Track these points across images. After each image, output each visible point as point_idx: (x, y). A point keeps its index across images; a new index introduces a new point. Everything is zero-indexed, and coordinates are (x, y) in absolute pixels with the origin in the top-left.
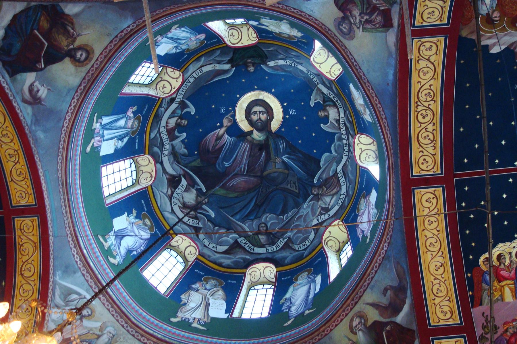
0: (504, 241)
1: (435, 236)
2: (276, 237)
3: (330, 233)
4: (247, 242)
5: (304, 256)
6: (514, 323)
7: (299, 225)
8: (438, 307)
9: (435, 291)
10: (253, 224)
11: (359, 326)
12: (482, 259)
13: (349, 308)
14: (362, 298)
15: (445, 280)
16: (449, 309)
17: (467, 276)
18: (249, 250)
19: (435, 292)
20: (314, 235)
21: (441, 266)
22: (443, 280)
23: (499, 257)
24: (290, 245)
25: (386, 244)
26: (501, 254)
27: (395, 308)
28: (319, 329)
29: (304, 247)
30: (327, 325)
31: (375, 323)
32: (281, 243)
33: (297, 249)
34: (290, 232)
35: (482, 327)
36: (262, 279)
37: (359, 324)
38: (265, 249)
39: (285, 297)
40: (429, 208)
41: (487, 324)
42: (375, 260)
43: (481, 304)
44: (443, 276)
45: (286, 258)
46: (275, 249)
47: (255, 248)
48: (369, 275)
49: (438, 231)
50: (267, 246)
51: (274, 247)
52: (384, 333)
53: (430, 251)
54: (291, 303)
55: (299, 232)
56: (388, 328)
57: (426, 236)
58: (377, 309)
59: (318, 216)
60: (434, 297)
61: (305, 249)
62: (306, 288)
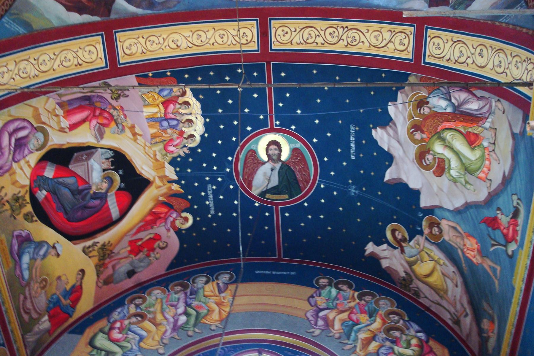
0: (203, 108)
1: (208, 40)
6: (122, 116)
8: (136, 41)
9: (152, 38)
15: (163, 49)
16: (134, 52)
19: (150, 39)
21: (177, 46)
22: (163, 47)
23: (187, 103)
26: (190, 104)
49: (213, 44)
53: (193, 34)
57: (208, 31)
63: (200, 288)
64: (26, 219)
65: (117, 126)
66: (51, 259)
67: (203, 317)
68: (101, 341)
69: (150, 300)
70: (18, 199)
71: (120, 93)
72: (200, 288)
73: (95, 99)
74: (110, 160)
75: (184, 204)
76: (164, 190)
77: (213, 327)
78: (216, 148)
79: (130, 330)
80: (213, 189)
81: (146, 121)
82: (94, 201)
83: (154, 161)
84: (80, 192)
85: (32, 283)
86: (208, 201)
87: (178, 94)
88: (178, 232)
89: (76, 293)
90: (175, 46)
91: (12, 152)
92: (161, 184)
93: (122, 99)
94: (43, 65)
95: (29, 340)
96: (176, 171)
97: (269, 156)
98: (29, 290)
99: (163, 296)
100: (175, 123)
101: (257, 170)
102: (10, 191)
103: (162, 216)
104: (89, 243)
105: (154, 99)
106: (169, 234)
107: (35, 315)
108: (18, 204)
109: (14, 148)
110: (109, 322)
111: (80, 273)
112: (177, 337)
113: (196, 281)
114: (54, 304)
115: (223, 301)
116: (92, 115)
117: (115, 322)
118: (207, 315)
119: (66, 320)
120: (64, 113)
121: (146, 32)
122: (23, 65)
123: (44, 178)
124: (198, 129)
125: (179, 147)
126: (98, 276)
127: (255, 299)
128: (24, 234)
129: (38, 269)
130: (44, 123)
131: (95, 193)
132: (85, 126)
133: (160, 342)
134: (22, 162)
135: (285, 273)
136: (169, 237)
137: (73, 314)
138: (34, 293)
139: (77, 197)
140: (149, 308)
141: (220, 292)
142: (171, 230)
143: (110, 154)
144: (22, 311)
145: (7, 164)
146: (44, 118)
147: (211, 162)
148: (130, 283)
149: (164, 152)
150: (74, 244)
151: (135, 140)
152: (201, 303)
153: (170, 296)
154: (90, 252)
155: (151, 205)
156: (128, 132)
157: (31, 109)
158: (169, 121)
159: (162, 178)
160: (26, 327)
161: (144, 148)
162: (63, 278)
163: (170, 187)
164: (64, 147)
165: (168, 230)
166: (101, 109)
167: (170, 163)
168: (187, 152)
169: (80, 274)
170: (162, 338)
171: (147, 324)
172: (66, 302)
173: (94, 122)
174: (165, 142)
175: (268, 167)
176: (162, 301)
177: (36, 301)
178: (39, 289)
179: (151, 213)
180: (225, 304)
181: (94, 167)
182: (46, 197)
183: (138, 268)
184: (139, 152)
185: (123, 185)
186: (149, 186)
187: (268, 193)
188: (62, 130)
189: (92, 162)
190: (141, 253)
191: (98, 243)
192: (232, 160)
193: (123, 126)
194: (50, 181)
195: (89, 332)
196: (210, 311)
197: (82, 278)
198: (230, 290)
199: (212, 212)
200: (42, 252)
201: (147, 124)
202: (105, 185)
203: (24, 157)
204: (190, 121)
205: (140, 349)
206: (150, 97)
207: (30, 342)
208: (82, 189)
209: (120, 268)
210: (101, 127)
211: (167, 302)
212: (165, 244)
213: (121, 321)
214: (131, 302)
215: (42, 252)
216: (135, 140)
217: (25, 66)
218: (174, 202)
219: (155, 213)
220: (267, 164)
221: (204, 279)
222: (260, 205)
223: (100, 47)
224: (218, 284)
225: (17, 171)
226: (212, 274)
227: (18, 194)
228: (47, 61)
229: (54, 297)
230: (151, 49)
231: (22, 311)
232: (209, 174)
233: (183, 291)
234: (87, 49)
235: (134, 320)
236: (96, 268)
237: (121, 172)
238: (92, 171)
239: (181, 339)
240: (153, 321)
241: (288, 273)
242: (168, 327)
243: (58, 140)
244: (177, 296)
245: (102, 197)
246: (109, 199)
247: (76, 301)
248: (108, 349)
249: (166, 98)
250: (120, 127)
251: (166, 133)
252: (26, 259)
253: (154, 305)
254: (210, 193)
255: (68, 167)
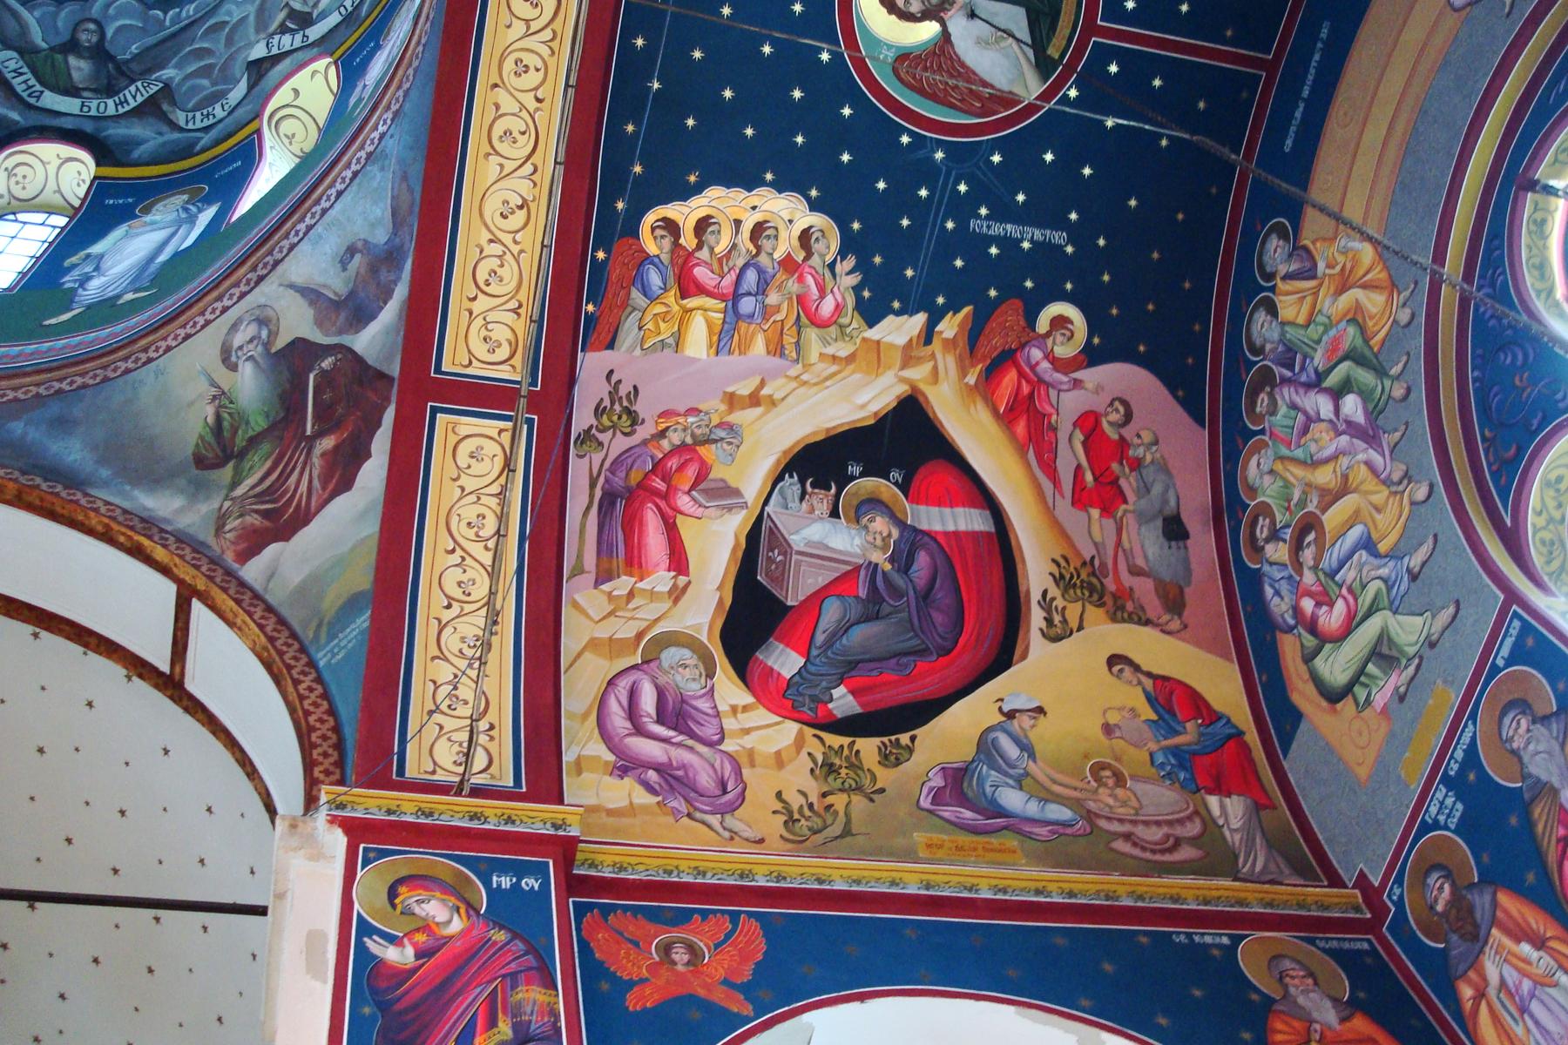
0: (728, 183)
1: (524, 114)
2: (123, 74)
3: (296, 92)
4: (25, 70)
5: (198, 148)
6: (691, 419)
7: (208, 52)
8: (479, 322)
9: (482, 276)
10: (56, 14)
11: (251, 347)
12: (650, 218)
13: (236, 291)
14: (280, 268)
15: (522, 251)
16: (509, 335)
17: (593, 257)
18: (24, 95)
19: (481, 279)
20: (244, 91)
21: (521, 207)
23: (703, 225)
24: (165, 107)
25: (389, 115)
26: (710, 217)
27: (358, 312)
28: (133, 342)
29: (206, 123)
30: (162, 332)
31: (299, 344)
32: (135, 95)
33: (182, 123)
34: (175, 67)
35: (596, 409)
36: (49, 196)
37: (251, 341)
38: (78, 102)
39: (89, 251)
40: (527, 21)
41: (612, 403)
42: (345, 159)
43: (611, 345)
44: (518, 237)
45: (139, 143)
46: (111, 111)
47: (47, 93)
48: (318, 202)
49: (539, 100)
50: (85, 94)
51: (110, 102)
52: (312, 377)
53: (498, 154)
54: (97, 269)
55: (205, 71)
56: (327, 364)
57: (497, 107)
58: (312, 303)
59: (271, 35)
60: (473, 292)
61: (206, 129)
62: (159, 236)
63: (1283, 333)
64: (898, 762)
65: (715, 441)
66: (1042, 733)
67: (1366, 341)
68: (1336, 666)
69: (1269, 492)
70: (832, 765)
71: (621, 408)
72: (1283, 333)
73: (618, 481)
74: (809, 489)
75: (1010, 315)
76: (948, 363)
77: (1404, 317)
78: (861, 175)
79: (1332, 575)
80: (987, 217)
81: (724, 358)
82: (915, 567)
83: (852, 367)
84: (874, 595)
85: (1092, 805)
86: (1022, 240)
87: (667, 243)
88: (1092, 356)
89: (1173, 700)
90: (522, 214)
91: (690, 742)
92: (928, 366)
93: (639, 407)
94: (470, 589)
95: (1258, 868)
96: (898, 313)
97: (926, 15)
98: (1109, 819)
99: (1270, 452)
100: (751, 276)
101: (963, 65)
102: (799, 781)
103: (1026, 389)
104: (1037, 617)
105: (664, 317)
106: (1089, 385)
107: (1193, 829)
108: (843, 771)
109: (681, 733)
110: (1290, 629)
111: (1116, 669)
112: (1397, 435)
113: (1258, 342)
114: (1182, 766)
115: (1338, 268)
116: (662, 504)
117: (1297, 610)
118: (1362, 330)
119: (1246, 748)
120: (631, 575)
121: (460, 287)
122: (451, 641)
123: (797, 678)
124: (788, 212)
125: (829, 283)
126: (1147, 623)
127: (1365, 165)
128: (938, 782)
129: (1058, 777)
130: (640, 636)
131: (892, 560)
132: (686, 527)
133: (1394, 489)
134: (729, 724)
135: (1317, 57)
136: (1099, 389)
137: (1235, 727)
138: (1121, 810)
139: (886, 609)
140: (1289, 501)
141: (1309, 273)
142: (1077, 375)
143: (791, 484)
144: (1167, 858)
145: (717, 765)
146: (627, 631)
147: (901, 198)
148: (1202, 542)
149: (833, 330)
150: (1024, 657)
151: (772, 403)
152: (1325, 339)
153: (1278, 430)
154: (1065, 621)
155: (983, 414)
156: (741, 417)
157: (587, 655)
158: (741, 291)
159: (908, 356)
160: (1216, 858)
161: (805, 383)
162: (1113, 718)
163: (946, 342)
164: (728, 602)
165: (1077, 384)
166: (653, 471)
167: (871, 322)
168: (850, 262)
169: (1121, 671)
170: (1387, 482)
171: (1332, 518)
172: (1190, 733)
173: (683, 501)
174: (804, 319)
175: (959, 25)
176: (1282, 458)
177: (1150, 811)
178: (1119, 791)
179: (1007, 419)
180: (1348, 266)
181: (816, 538)
182: (853, 692)
183: (1165, 502)
184: (814, 399)
185: (896, 475)
186: (921, 399)
187: (1045, 50)
188: (677, 594)
189: (797, 540)
190: (1122, 482)
191: (1045, 593)
192: (911, 133)
193: (720, 425)
194: (812, 669)
195: (1303, 696)
196: (1356, 317)
197: (1137, 668)
198: (1314, 243)
199: (1059, 237)
200: (1012, 751)
201: (735, 357)
202: (880, 524)
203: (718, 715)
204: (758, 230)
205: (1394, 555)
206: (657, 326)
207: (1265, 867)
208: (869, 591)
209: (1146, 557)
210: (702, 486)
211: (1289, 445)
212: (1117, 404)
213: (1299, 591)
214: (1258, 550)
215: (1012, 751)
216: (772, 403)
217: (457, 636)
218: (995, 342)
219: (1011, 409)
220: (951, 29)
221: (1261, 316)
222: (1078, 85)
223: (468, 425)
224: (1288, 277)
225: (749, 746)
226: (1253, 289)
227: (814, 761)
228: (464, 578)
229: (1160, 759)
230: (514, 284)
231: (1167, 858)
232: (936, 215)
233: (1273, 387)
234: (463, 460)
235: (1308, 555)
236: (1123, 621)
237: (854, 469)
238: (827, 548)
239: (1407, 424)
240: (1330, 497)
241: (1320, 45)
242: (1361, 457)
243: (702, 609)
244: (1282, 408)
245: (912, 541)
246: (924, 526)
247: (1196, 704)
248: (1366, 651)
249: (671, 281)
250: (721, 433)
251: (778, 309)
252: (1012, 799)
253: (1287, 485)
254: (997, 229)
255: (792, 607)
